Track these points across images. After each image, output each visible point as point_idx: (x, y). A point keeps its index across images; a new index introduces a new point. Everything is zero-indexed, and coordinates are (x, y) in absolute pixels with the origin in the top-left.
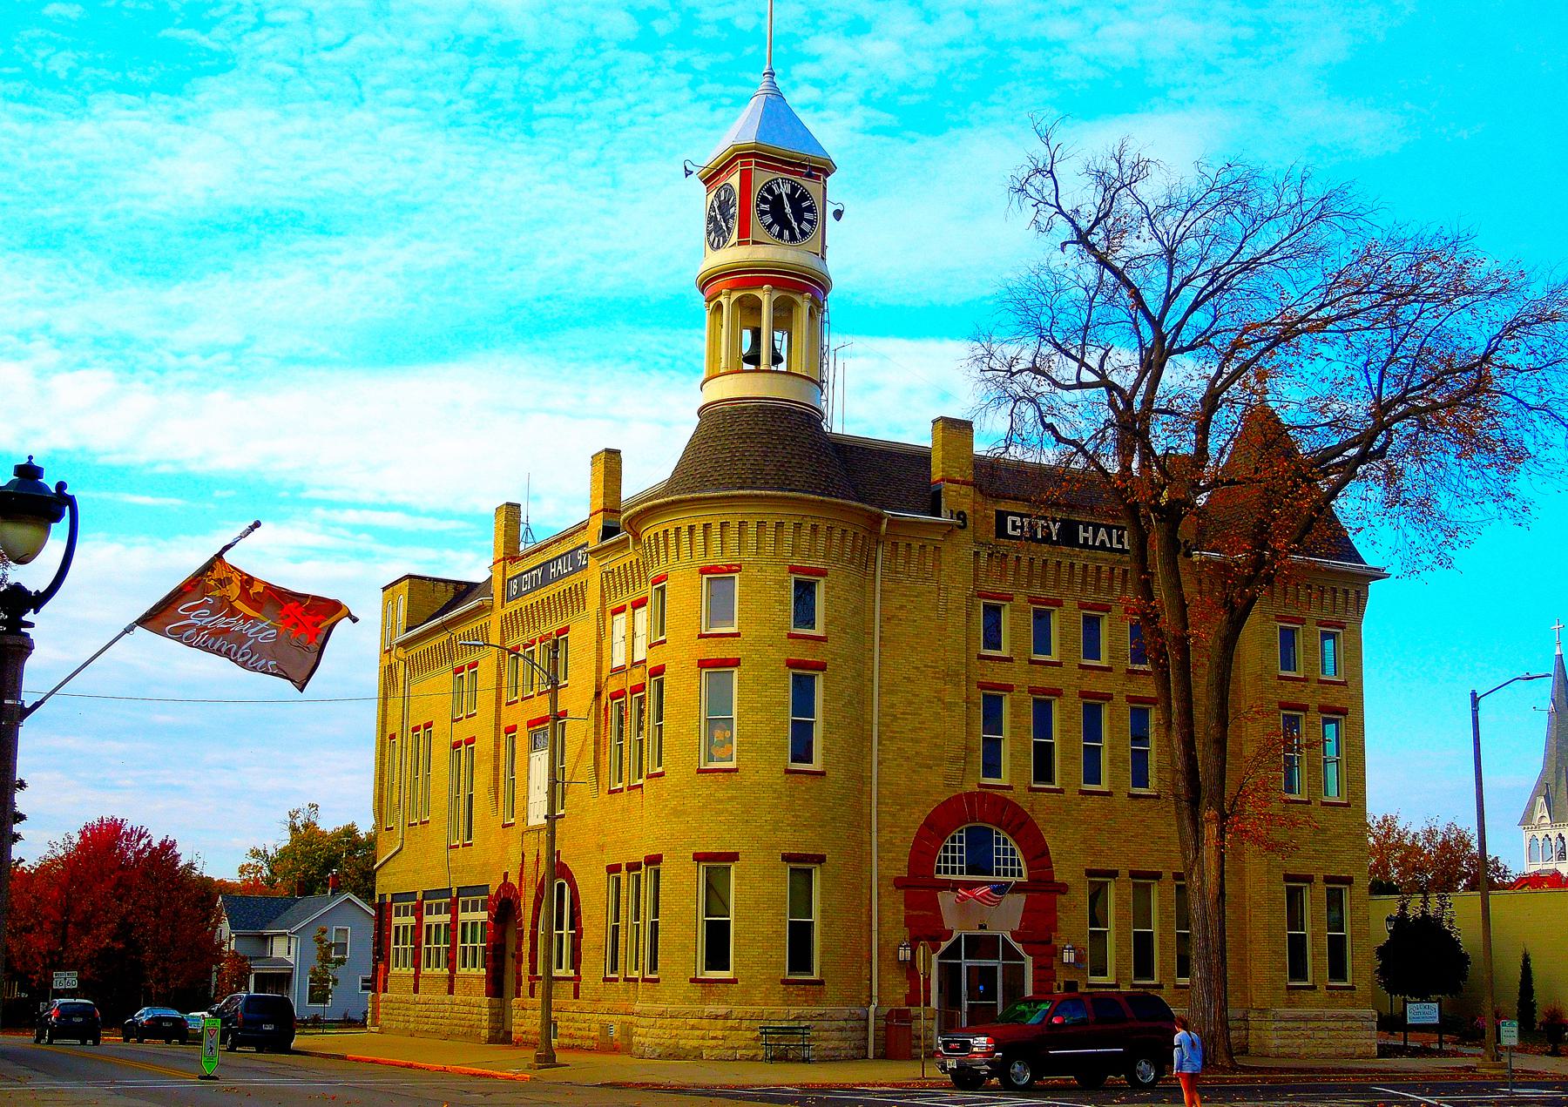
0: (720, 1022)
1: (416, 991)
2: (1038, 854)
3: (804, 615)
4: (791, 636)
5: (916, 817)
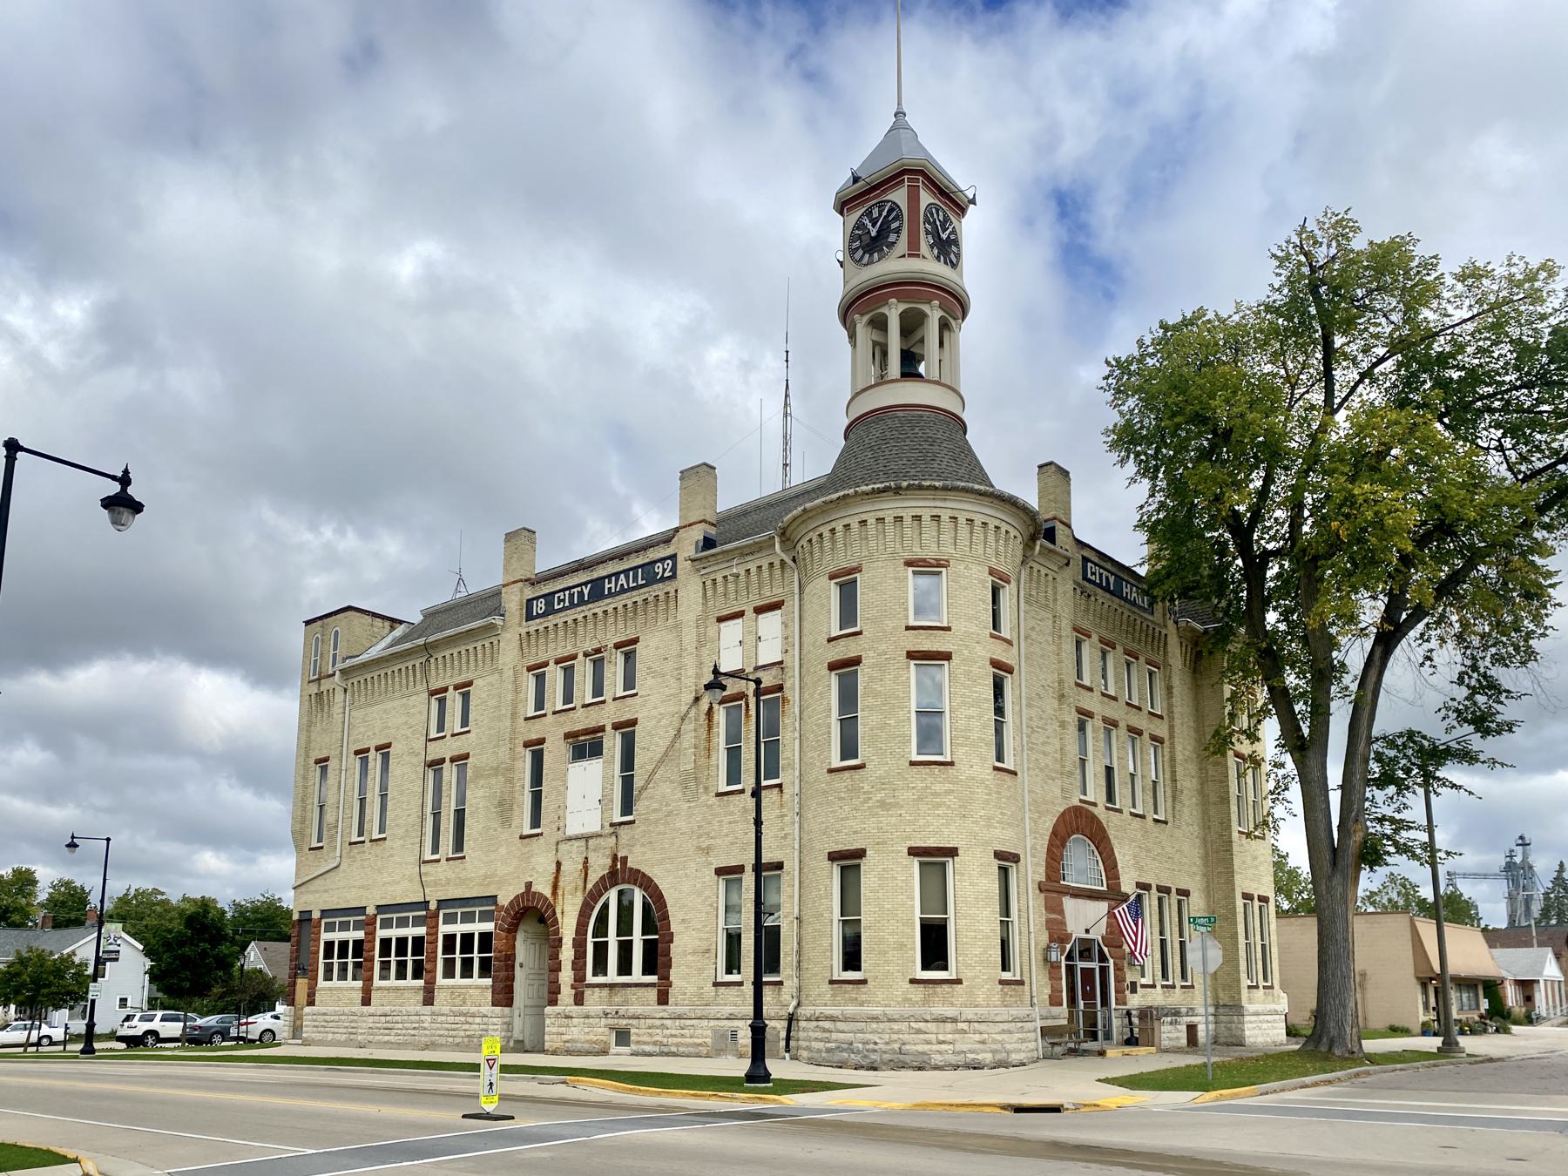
0: (949, 1026)
5: (1048, 824)
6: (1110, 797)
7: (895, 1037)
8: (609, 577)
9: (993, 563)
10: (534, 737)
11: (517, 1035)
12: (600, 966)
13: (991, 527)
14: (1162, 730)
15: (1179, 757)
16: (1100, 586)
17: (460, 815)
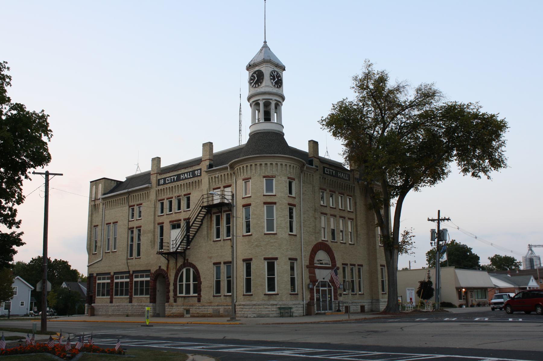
5: (310, 248)
6: (334, 238)
8: (182, 174)
10: (161, 222)
11: (157, 312)
12: (181, 292)
13: (288, 165)
14: (352, 216)
15: (359, 224)
16: (330, 175)
17: (139, 245)
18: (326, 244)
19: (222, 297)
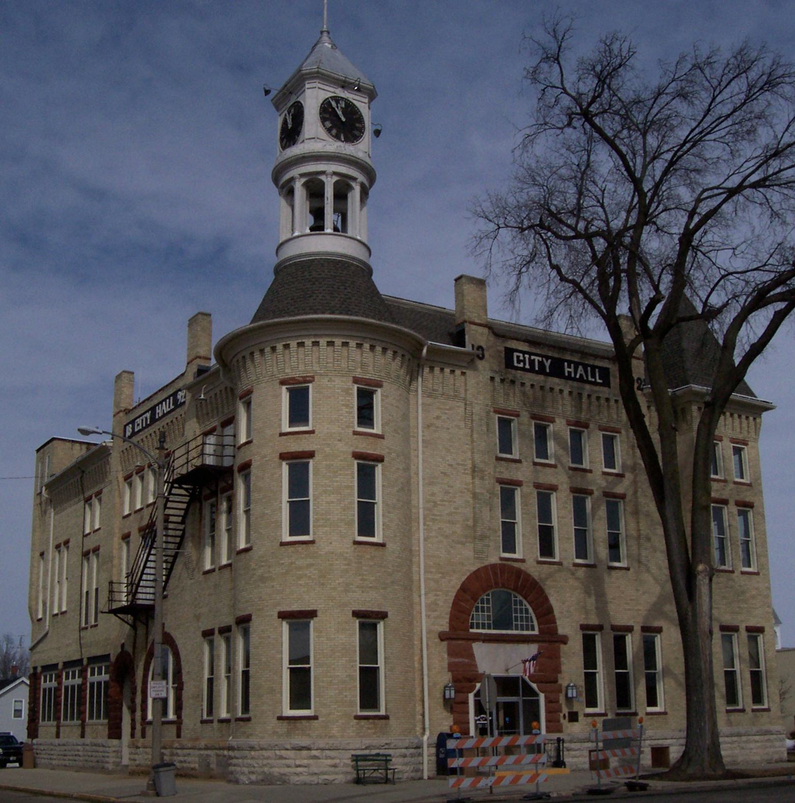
0: (304, 753)
1: (58, 736)
2: (545, 613)
3: (365, 415)
4: (356, 433)
5: (455, 582)
7: (265, 762)
9: (359, 373)
18: (519, 572)
19: (216, 724)
